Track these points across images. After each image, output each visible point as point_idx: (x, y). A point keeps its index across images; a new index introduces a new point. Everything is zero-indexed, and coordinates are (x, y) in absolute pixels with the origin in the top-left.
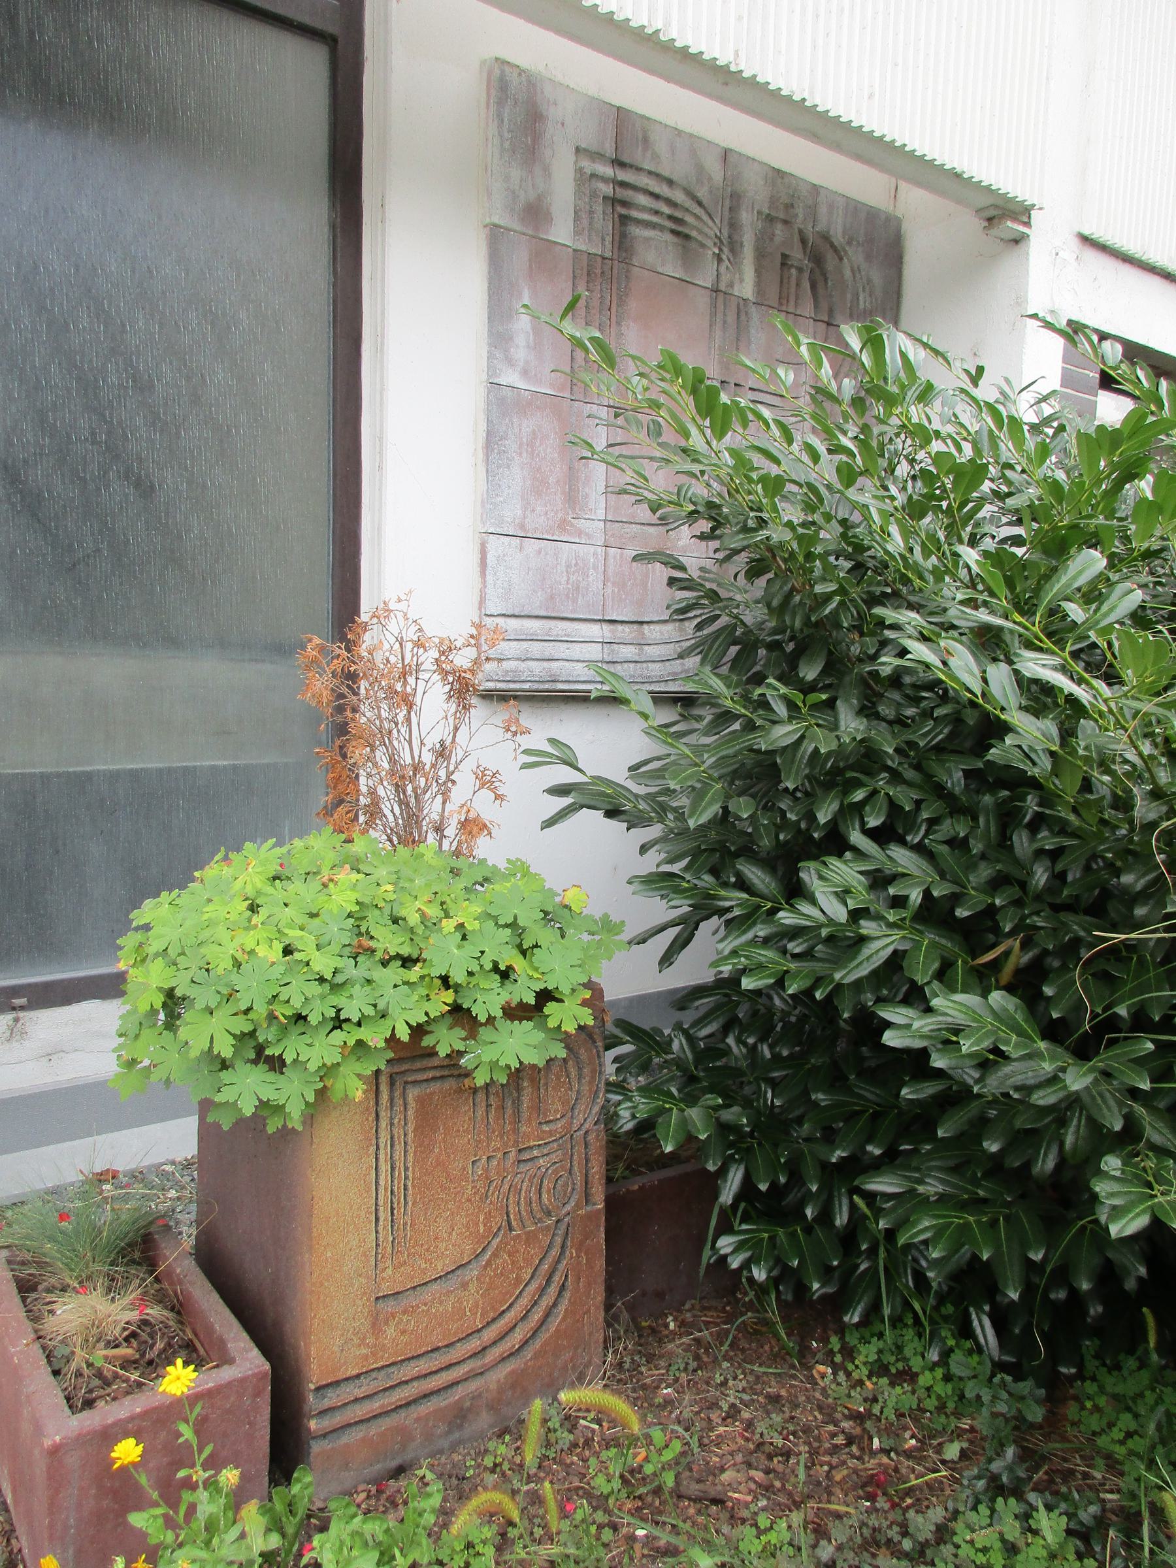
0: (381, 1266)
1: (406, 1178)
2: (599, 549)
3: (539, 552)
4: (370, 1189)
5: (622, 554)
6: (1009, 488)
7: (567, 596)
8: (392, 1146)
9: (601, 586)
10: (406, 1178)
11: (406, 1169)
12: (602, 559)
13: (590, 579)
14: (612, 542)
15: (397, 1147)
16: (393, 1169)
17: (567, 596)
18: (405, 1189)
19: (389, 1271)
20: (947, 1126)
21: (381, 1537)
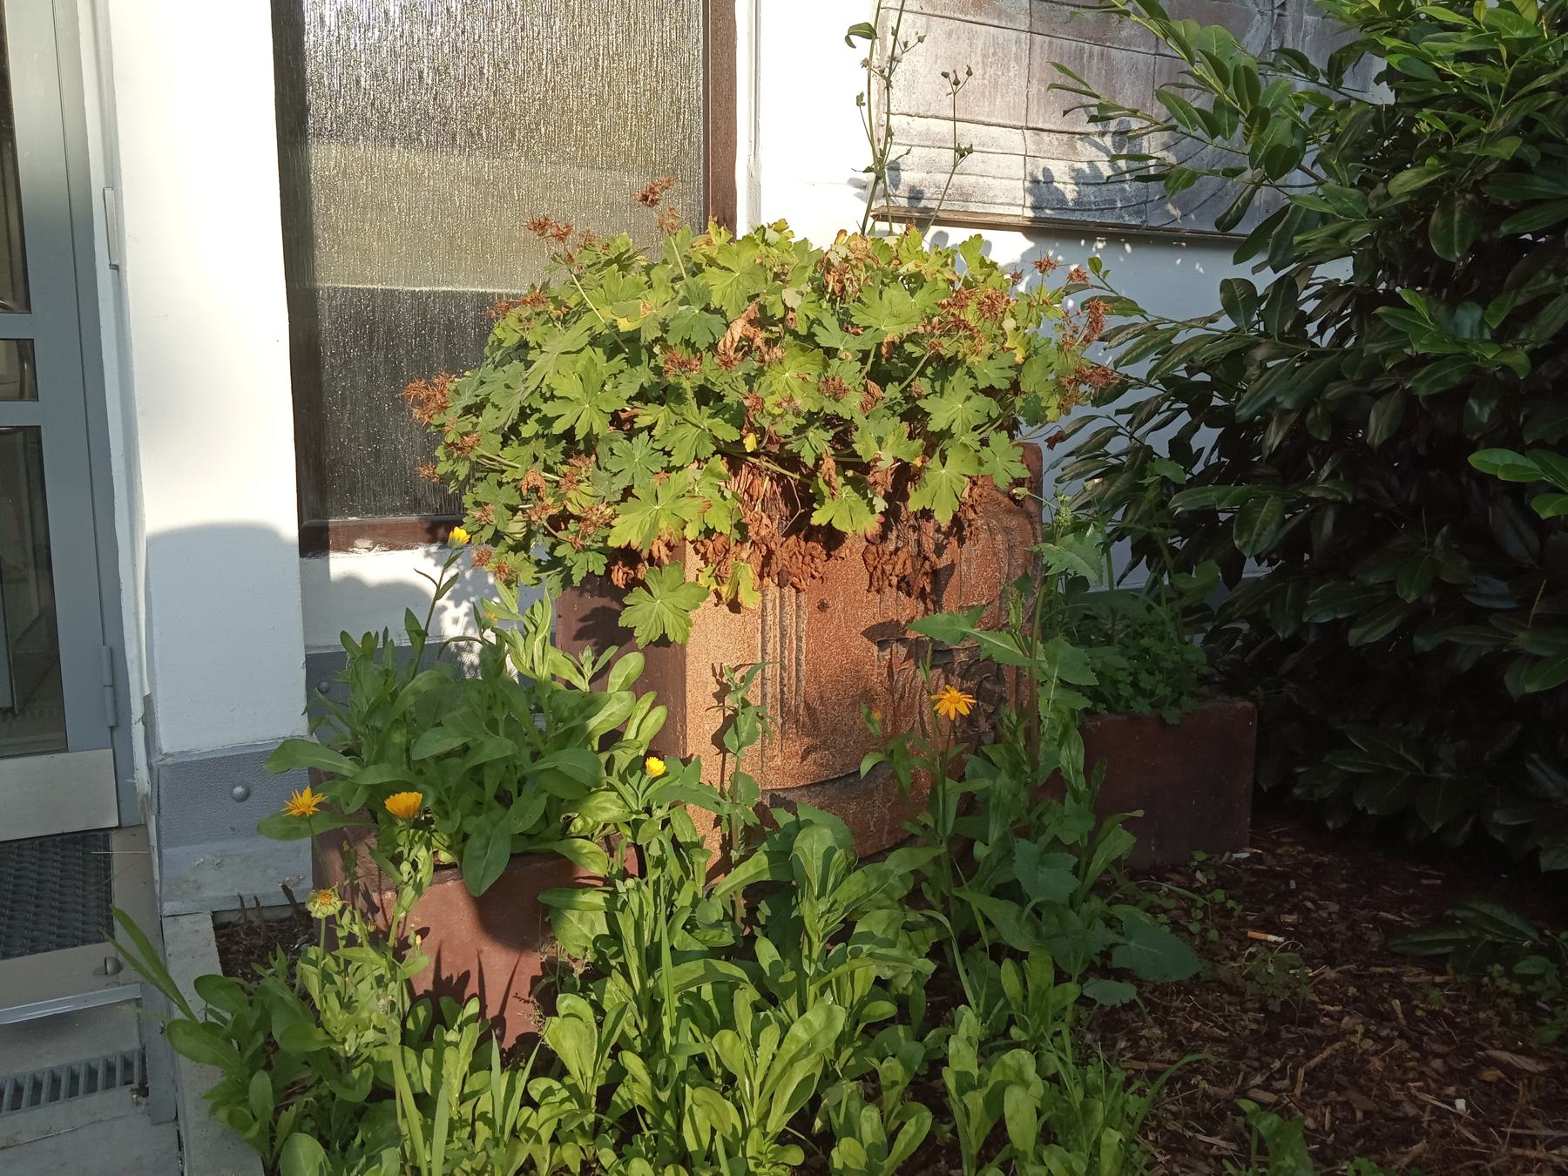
0: (769, 753)
1: (799, 649)
2: (1023, 35)
3: (950, 35)
4: (715, 100)
5: (1051, 44)
6: (1350, 334)
7: (983, 93)
8: (782, 607)
9: (1024, 84)
10: (799, 649)
11: (799, 639)
12: (1025, 47)
13: (1012, 74)
14: (1038, 27)
15: (787, 608)
16: (783, 636)
17: (983, 93)
18: (798, 664)
19: (778, 761)
20: (879, 1012)
21: (1209, 108)
